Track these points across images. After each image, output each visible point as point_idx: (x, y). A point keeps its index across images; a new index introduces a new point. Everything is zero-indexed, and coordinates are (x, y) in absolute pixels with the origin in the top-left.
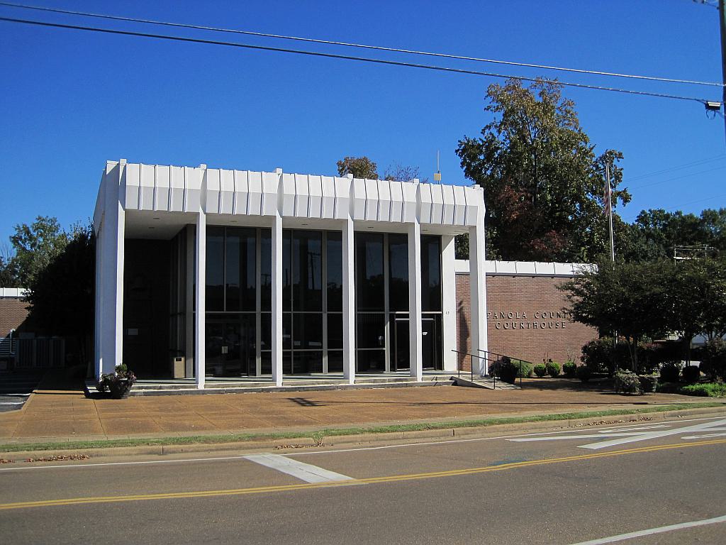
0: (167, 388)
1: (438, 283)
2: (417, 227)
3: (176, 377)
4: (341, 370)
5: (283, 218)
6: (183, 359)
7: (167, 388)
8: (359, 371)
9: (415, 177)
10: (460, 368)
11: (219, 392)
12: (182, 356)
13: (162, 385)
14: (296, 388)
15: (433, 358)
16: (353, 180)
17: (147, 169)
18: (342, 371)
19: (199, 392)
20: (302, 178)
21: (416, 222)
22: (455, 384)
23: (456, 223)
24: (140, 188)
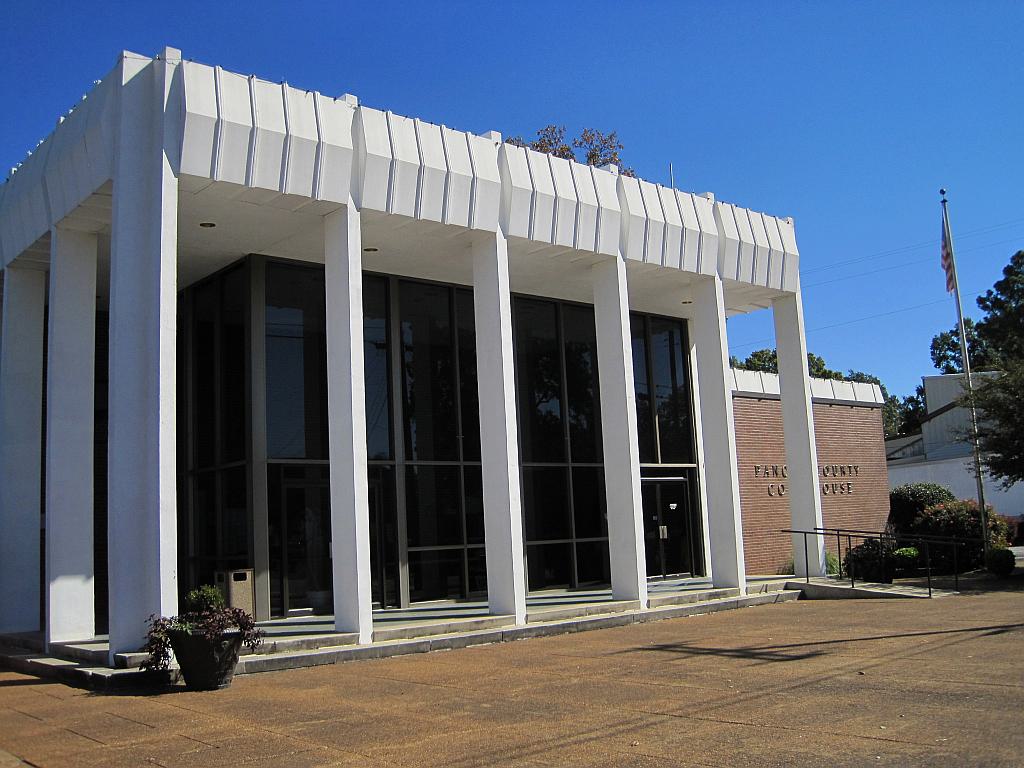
0: (289, 647)
1: (680, 382)
2: (502, 245)
3: (55, 638)
4: (326, 608)
5: (367, 217)
6: (249, 575)
7: (289, 647)
8: (604, 583)
9: (612, 161)
10: (102, 624)
11: (416, 649)
12: (246, 567)
13: (278, 640)
14: (563, 626)
15: (676, 549)
16: (180, 65)
17: (233, 84)
18: (332, 613)
19: (738, 605)
20: (402, 125)
21: (717, 278)
22: (802, 597)
23: (741, 279)
24: (421, 169)
